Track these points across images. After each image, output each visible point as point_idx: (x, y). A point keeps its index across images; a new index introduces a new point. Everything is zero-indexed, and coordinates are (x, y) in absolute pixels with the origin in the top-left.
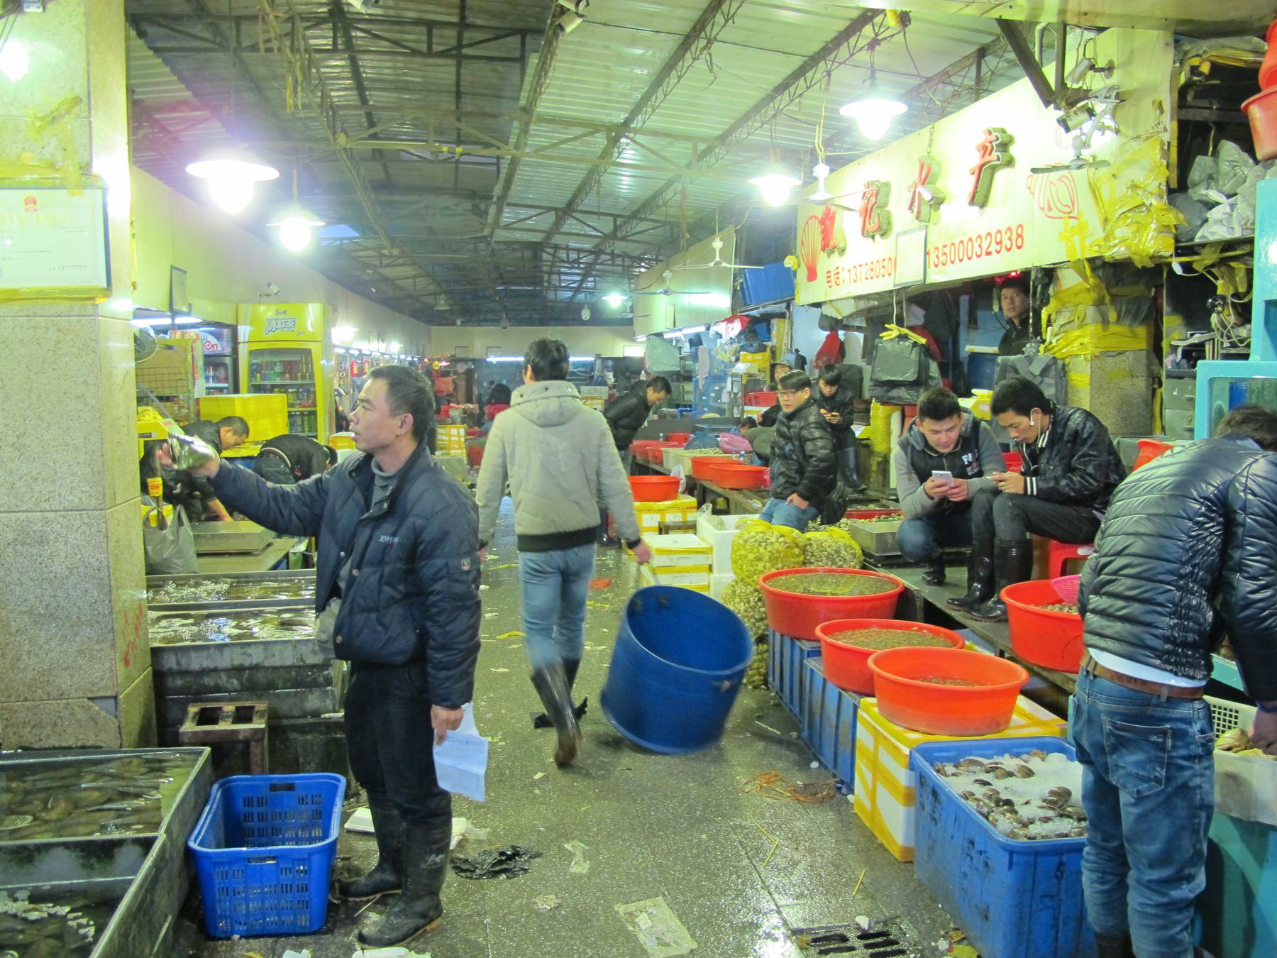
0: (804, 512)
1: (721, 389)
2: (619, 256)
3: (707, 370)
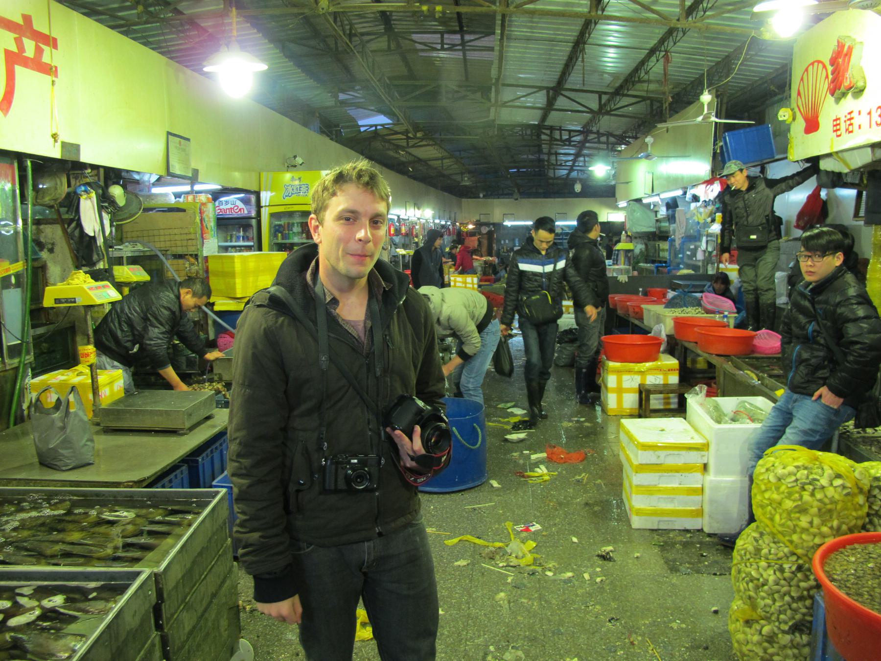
0: (836, 412)
1: (696, 249)
2: (603, 135)
3: (683, 230)
